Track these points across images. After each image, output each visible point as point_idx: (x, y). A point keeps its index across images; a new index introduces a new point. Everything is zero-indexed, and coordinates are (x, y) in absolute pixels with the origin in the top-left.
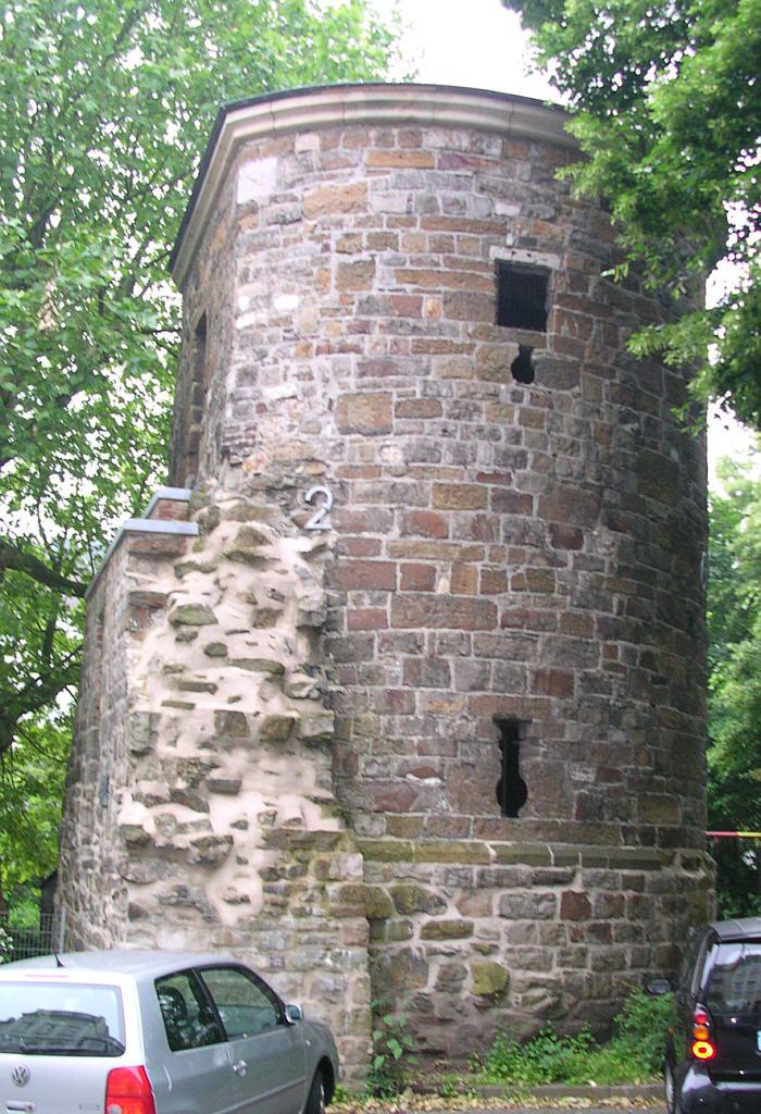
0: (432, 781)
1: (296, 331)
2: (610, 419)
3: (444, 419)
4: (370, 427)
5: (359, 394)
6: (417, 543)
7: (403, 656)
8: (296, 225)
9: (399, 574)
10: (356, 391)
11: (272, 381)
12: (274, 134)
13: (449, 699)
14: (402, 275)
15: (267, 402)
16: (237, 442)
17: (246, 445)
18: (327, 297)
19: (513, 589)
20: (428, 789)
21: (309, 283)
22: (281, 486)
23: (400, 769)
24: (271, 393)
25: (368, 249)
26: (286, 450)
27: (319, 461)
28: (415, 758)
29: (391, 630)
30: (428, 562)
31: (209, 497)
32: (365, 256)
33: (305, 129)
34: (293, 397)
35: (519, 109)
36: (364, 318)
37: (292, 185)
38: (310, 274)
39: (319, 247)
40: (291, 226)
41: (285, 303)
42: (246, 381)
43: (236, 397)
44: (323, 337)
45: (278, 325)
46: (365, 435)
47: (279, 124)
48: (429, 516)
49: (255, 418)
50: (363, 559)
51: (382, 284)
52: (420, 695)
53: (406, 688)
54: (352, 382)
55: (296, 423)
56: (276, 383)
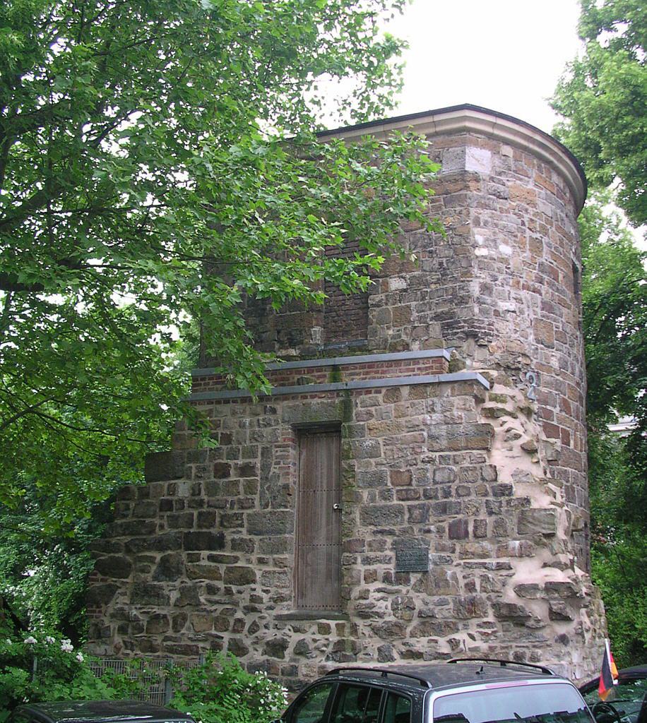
2: (509, 381)
8: (505, 201)
12: (490, 136)
14: (556, 258)
15: (501, 310)
16: (483, 331)
17: (490, 335)
21: (515, 241)
22: (513, 367)
24: (503, 305)
26: (513, 345)
27: (528, 356)
31: (333, 371)
32: (538, 235)
33: (560, 173)
34: (513, 312)
37: (500, 174)
38: (516, 236)
39: (520, 221)
40: (501, 200)
41: (506, 250)
43: (481, 301)
47: (497, 132)
50: (549, 421)
51: (545, 257)
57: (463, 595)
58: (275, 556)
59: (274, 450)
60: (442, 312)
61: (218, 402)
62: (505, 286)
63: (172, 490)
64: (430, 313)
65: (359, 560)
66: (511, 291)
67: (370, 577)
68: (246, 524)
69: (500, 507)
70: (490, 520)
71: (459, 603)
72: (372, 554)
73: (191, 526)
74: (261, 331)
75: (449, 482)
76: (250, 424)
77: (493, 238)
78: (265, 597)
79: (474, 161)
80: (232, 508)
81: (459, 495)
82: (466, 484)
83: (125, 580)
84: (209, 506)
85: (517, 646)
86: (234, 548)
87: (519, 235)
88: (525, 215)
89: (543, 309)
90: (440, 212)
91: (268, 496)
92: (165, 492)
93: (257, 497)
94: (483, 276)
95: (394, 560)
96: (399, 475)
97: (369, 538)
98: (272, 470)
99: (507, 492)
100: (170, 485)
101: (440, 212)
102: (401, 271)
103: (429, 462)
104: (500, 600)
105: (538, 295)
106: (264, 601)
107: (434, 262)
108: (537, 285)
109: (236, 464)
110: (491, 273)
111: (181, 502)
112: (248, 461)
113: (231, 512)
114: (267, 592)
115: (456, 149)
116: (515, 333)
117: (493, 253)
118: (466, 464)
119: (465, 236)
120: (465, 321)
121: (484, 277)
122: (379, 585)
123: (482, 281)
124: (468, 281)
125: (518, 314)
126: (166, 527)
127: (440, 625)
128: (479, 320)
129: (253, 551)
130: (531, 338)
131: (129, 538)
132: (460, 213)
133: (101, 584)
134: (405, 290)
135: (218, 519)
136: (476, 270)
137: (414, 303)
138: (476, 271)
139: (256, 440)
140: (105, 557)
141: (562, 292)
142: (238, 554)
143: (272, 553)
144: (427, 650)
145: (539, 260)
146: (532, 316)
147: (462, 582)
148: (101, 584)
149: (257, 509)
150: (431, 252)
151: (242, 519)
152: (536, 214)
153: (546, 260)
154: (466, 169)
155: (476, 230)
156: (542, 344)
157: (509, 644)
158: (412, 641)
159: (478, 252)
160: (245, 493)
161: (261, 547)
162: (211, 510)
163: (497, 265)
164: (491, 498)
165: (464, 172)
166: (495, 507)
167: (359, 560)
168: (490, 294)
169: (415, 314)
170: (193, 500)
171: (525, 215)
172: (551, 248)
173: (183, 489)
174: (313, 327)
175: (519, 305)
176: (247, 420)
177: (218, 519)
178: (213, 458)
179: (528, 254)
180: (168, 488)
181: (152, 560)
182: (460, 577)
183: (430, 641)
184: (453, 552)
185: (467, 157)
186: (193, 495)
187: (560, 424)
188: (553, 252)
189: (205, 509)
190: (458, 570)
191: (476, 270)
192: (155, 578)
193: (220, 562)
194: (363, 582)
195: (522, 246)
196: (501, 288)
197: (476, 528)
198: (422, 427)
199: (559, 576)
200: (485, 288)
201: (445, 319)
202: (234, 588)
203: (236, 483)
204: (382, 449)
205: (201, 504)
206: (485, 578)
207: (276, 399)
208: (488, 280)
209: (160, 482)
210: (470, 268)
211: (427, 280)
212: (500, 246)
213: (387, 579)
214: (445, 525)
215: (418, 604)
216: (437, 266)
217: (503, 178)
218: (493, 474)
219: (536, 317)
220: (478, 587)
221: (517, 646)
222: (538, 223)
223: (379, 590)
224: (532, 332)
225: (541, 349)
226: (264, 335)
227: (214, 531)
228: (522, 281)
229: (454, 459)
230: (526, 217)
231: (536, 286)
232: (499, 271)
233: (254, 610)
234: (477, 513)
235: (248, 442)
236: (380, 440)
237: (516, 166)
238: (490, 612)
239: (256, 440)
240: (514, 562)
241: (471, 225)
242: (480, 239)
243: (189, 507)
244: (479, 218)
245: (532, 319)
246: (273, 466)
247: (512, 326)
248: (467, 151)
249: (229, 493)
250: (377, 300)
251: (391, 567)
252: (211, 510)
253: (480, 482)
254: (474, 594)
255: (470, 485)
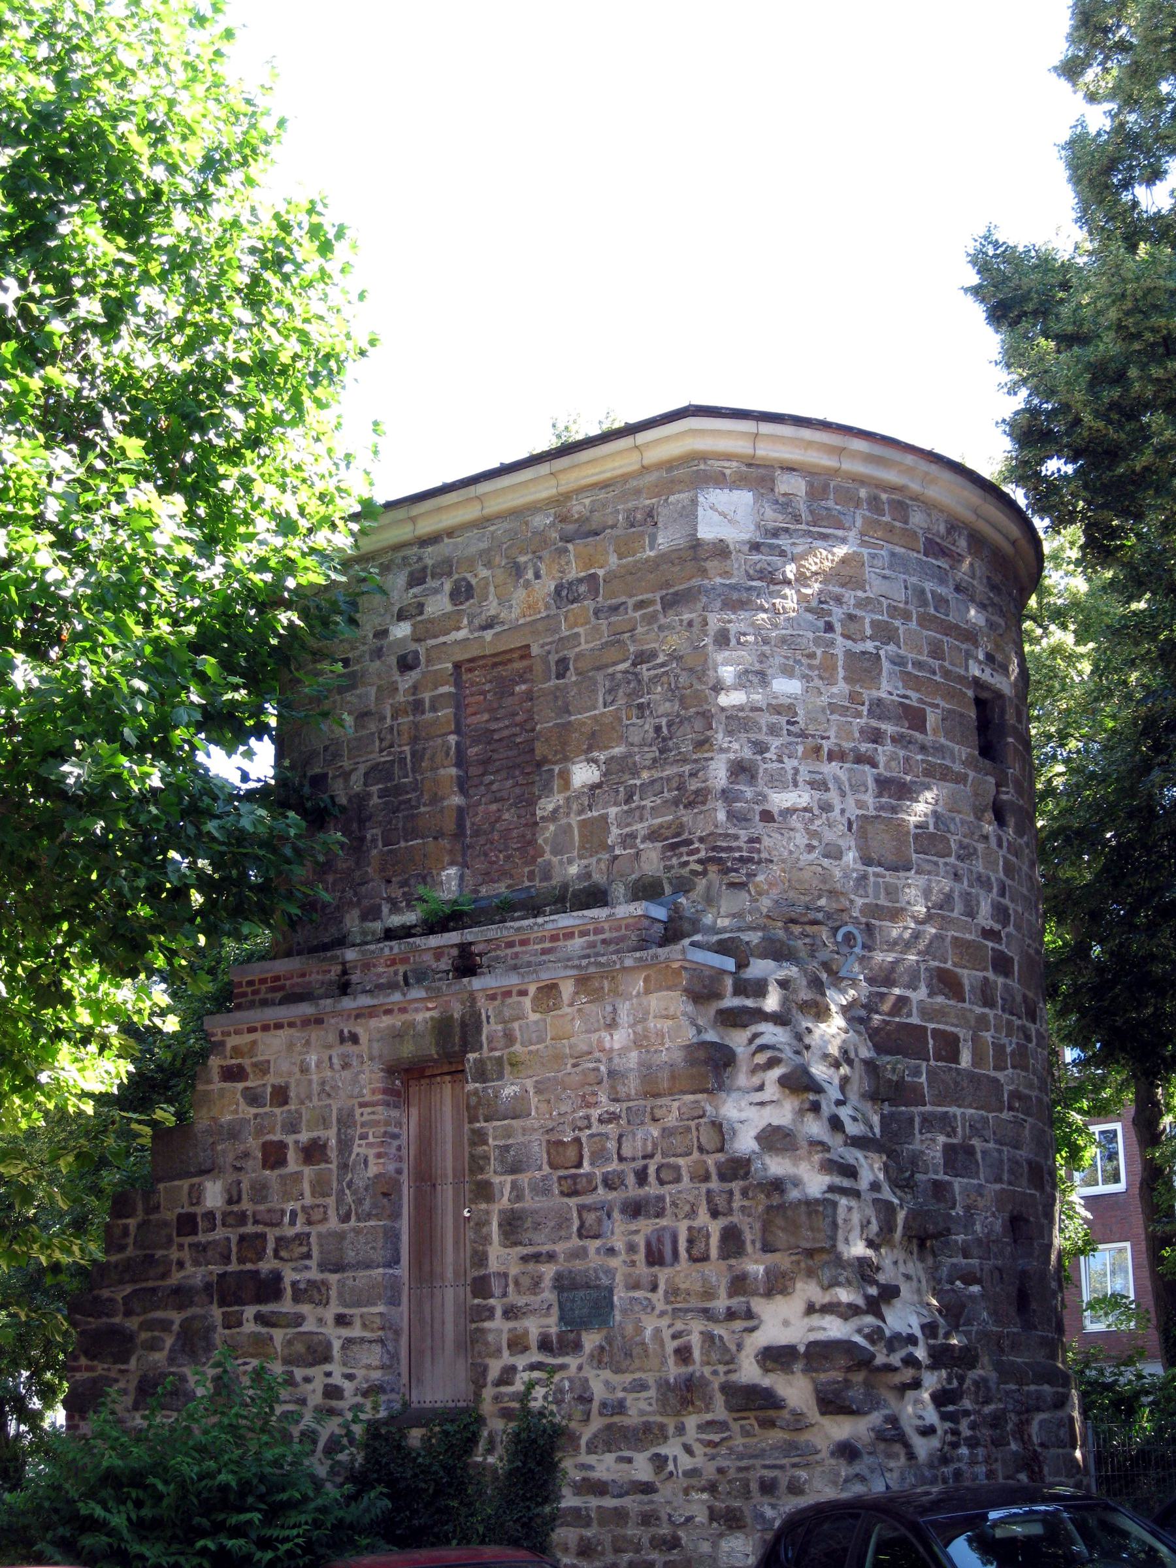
0: (975, 1289)
1: (802, 725)
3: (952, 860)
4: (890, 858)
5: (877, 817)
6: (943, 1006)
7: (942, 1139)
9: (931, 1041)
10: (874, 813)
11: (778, 781)
13: (979, 1189)
14: (909, 680)
15: (775, 811)
16: (737, 855)
17: (750, 860)
18: (835, 690)
19: (1014, 1067)
20: (971, 1297)
21: (810, 667)
22: (805, 919)
23: (949, 1275)
24: (780, 800)
25: (871, 638)
28: (959, 1260)
29: (928, 1108)
30: (953, 1029)
32: (869, 646)
34: (805, 810)
35: (806, 433)
36: (874, 723)
37: (775, 533)
39: (821, 624)
41: (786, 687)
42: (742, 777)
44: (833, 740)
45: (779, 713)
46: (887, 869)
48: (947, 971)
49: (759, 828)
51: (887, 688)
52: (958, 1184)
53: (947, 1178)
54: (869, 799)
55: (815, 843)
56: (785, 788)
57: (673, 1371)
58: (365, 1310)
59: (358, 1111)
60: (661, 826)
61: (266, 1028)
62: (786, 759)
63: (196, 1196)
64: (641, 828)
65: (499, 1313)
66: (801, 768)
67: (517, 1344)
68: (315, 1253)
69: (730, 1201)
70: (715, 1228)
71: (665, 1386)
72: (521, 1301)
73: (226, 1259)
74: (358, 880)
75: (644, 1157)
76: (317, 1066)
77: (757, 667)
78: (348, 1386)
79: (716, 517)
80: (293, 1223)
81: (662, 1183)
82: (672, 1160)
83: (123, 1367)
84: (256, 1222)
85: (765, 1467)
86: (296, 1299)
87: (819, 652)
88: (835, 610)
89: (880, 795)
90: (655, 626)
91: (349, 1198)
92: (185, 1199)
93: (331, 1201)
94: (736, 746)
95: (555, 1310)
96: (561, 1149)
97: (514, 1271)
98: (356, 1150)
99: (742, 1172)
100: (192, 1186)
101: (655, 626)
102: (590, 749)
103: (609, 1121)
104: (734, 1377)
105: (867, 768)
106: (346, 1394)
107: (647, 727)
108: (864, 747)
109: (297, 1142)
110: (753, 736)
111: (210, 1215)
112: (315, 1134)
113: (290, 1232)
114: (350, 1377)
115: (682, 496)
116: (809, 852)
117: (757, 697)
118: (671, 1120)
119: (700, 670)
120: (701, 840)
121: (740, 749)
122: (536, 1357)
123: (732, 756)
124: (707, 759)
125: (816, 812)
126: (188, 1264)
127: (635, 1430)
128: (727, 835)
129: (327, 1303)
130: (850, 857)
131: (128, 1289)
132: (690, 624)
133: (87, 1375)
134: (598, 786)
135: (271, 1245)
136: (720, 736)
137: (613, 811)
138: (720, 738)
139: (329, 1095)
140: (93, 1323)
141: (940, 750)
142: (305, 1309)
143: (358, 1304)
144: (615, 1477)
145: (869, 694)
146: (853, 812)
147: (671, 1346)
148: (87, 1375)
149: (333, 1223)
150: (640, 707)
151: (309, 1244)
152: (861, 604)
153: (890, 693)
154: (699, 535)
155: (720, 657)
156: (880, 865)
157: (751, 1462)
158: (591, 1459)
159: (724, 700)
160: (313, 1195)
161: (340, 1294)
162: (260, 1229)
163: (765, 719)
164: (714, 1184)
165: (696, 545)
166: (721, 1201)
167: (499, 1313)
168: (752, 780)
169: (615, 830)
170: (231, 1212)
171: (835, 610)
172: (904, 664)
173: (214, 1195)
174: (444, 869)
175: (817, 795)
176: (312, 1059)
177: (271, 1245)
178: (260, 1131)
179: (841, 687)
180: (190, 1193)
181: (165, 1325)
182: (667, 1334)
183: (621, 1460)
184: (654, 1288)
185: (700, 510)
186: (230, 1202)
187: (930, 1020)
188: (909, 673)
189: (250, 1229)
190: (664, 1322)
191: (720, 736)
192: (171, 1360)
193: (274, 1325)
194: (506, 1353)
195: (826, 675)
196: (776, 765)
197: (691, 1242)
198: (597, 1054)
199: (834, 1328)
200: (741, 770)
201: (666, 839)
202: (299, 1373)
203: (297, 1177)
204: (534, 1100)
205: (242, 1218)
206: (708, 1338)
207: (357, 1017)
208: (747, 753)
209: (176, 1183)
210: (709, 733)
211: (635, 763)
212: (775, 682)
213: (545, 1345)
214: (640, 1240)
215: (598, 1390)
216: (652, 734)
217: (783, 542)
218: (717, 1139)
219: (860, 812)
220: (697, 1354)
221: (765, 1467)
222: (867, 621)
223: (533, 1367)
224: (853, 844)
225: (876, 875)
226: (363, 889)
227: (266, 1265)
228: (826, 745)
229: (652, 1113)
230: (837, 613)
231: (863, 749)
232: (773, 730)
233: (332, 1412)
234: (692, 1214)
235: (315, 1099)
236: (529, 1084)
237: (811, 512)
238: (719, 1400)
239: (329, 1095)
240: (759, 1305)
241: (711, 648)
242: (727, 673)
243: (224, 1225)
244: (727, 630)
245: (853, 818)
246: (357, 1142)
247: (801, 839)
248: (701, 499)
249: (286, 1196)
250: (550, 807)
251: (552, 1325)
252: (260, 1229)
253: (696, 1155)
254: (690, 1369)
255: (681, 1161)
